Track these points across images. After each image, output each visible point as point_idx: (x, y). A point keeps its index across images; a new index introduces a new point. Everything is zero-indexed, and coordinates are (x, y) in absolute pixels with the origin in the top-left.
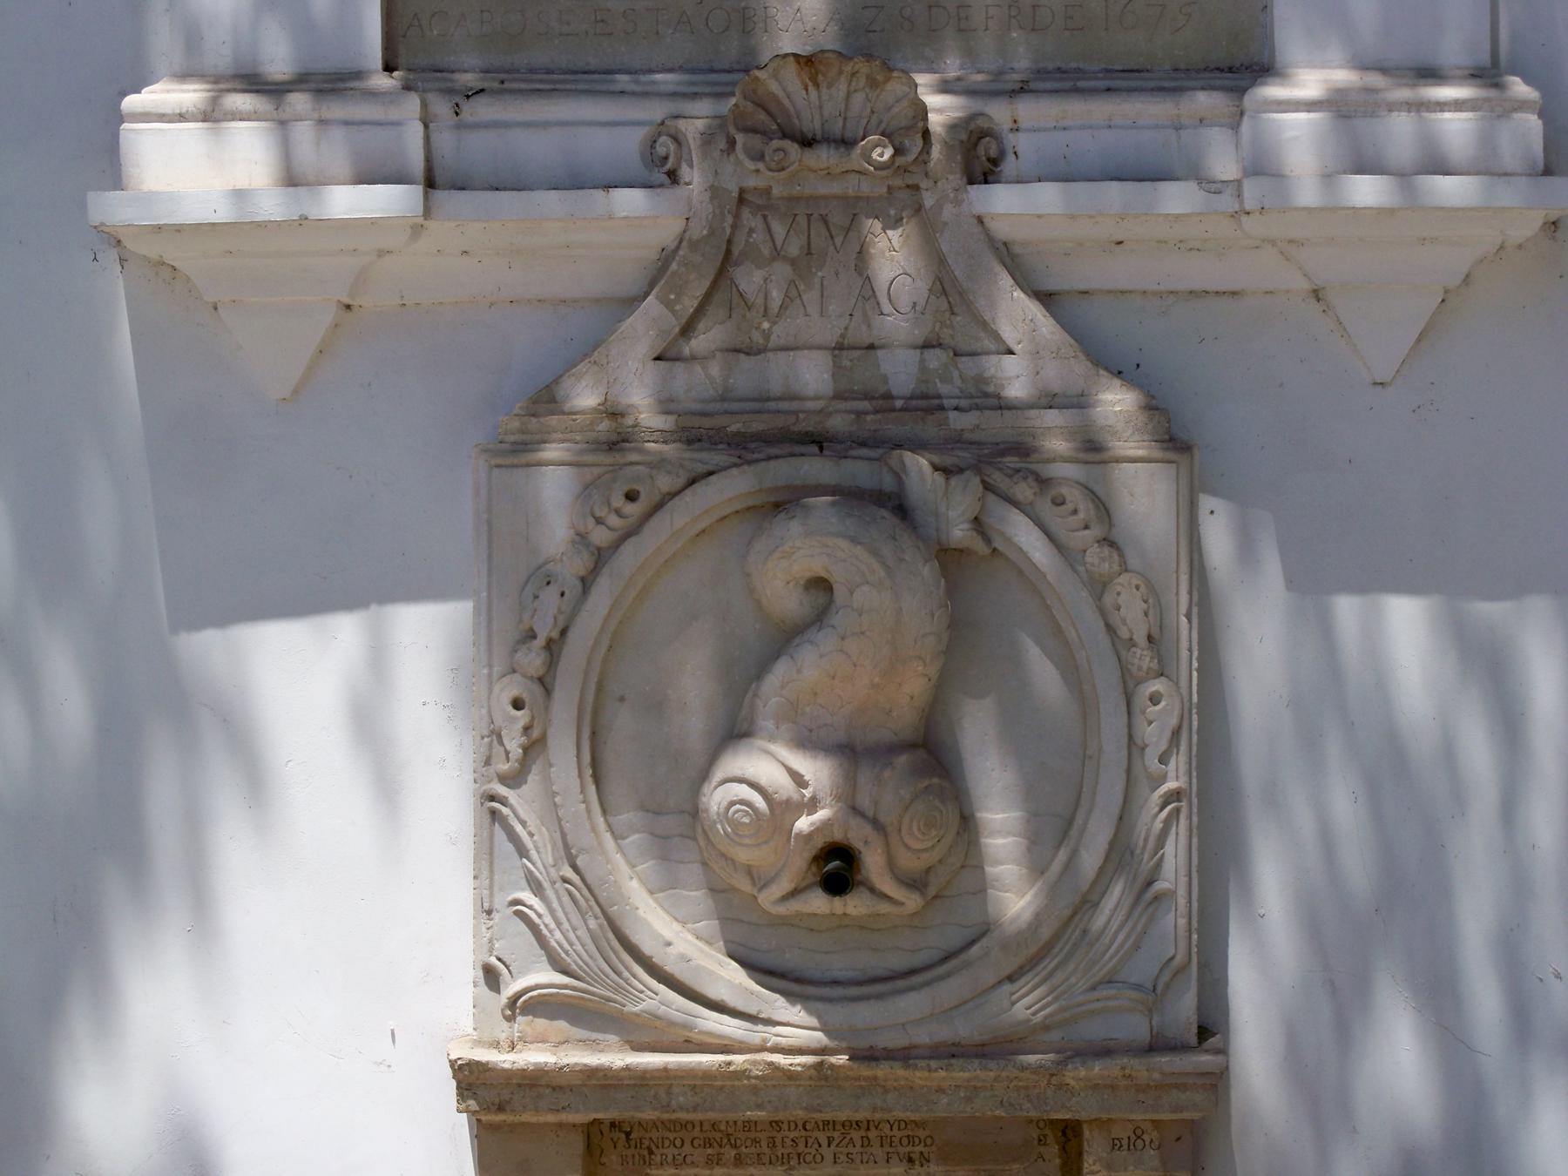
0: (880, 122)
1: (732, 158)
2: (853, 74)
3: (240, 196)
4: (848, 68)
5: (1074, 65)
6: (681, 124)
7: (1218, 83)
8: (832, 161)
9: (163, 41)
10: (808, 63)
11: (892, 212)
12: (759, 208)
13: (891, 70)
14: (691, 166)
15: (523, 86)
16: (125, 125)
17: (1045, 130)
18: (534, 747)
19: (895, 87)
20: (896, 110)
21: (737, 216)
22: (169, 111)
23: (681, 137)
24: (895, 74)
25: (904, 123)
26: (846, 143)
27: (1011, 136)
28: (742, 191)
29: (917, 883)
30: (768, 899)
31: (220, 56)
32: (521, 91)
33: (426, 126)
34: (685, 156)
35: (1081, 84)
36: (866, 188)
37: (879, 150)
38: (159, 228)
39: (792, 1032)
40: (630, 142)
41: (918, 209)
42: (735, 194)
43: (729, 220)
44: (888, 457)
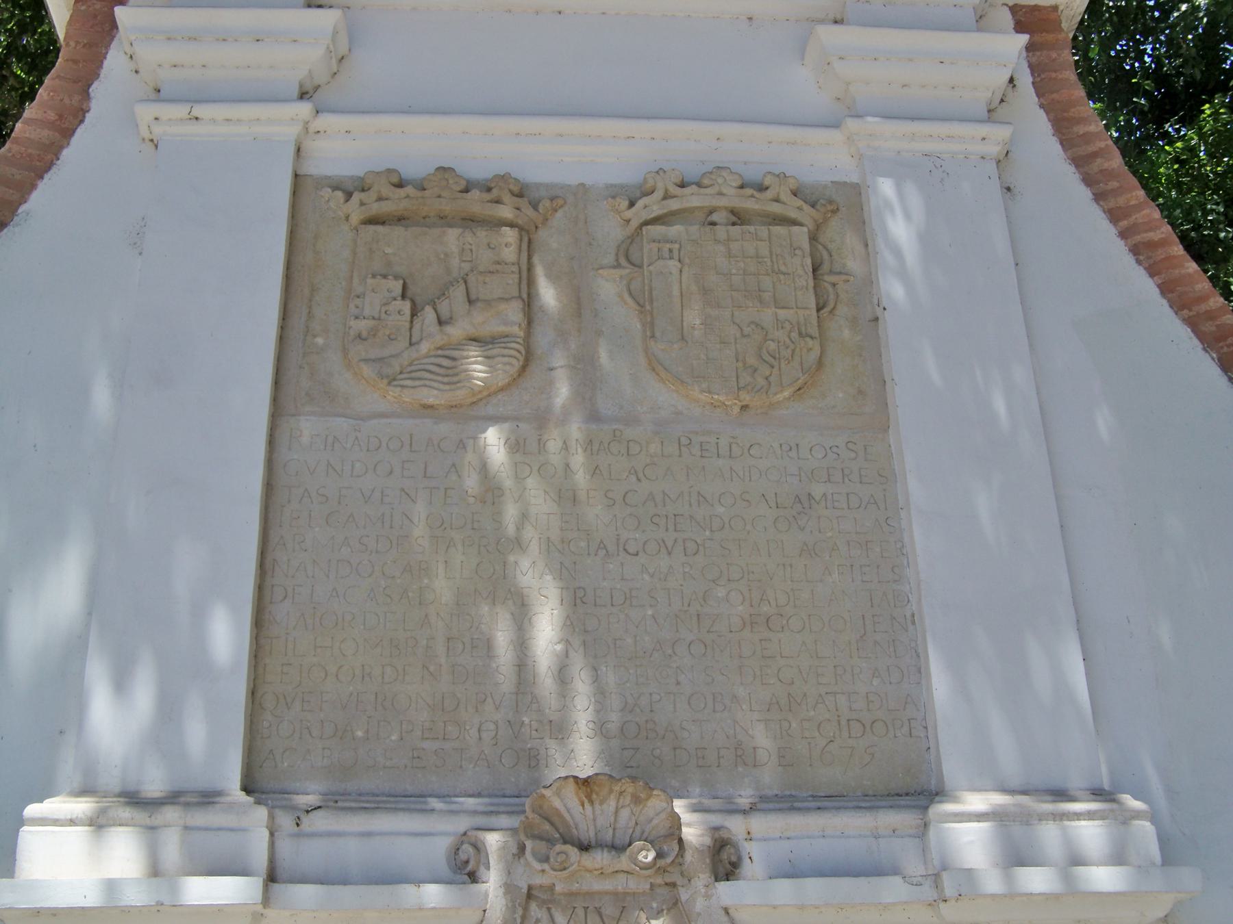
0: (643, 832)
1: (522, 860)
2: (621, 793)
3: (111, 886)
4: (617, 788)
5: (788, 793)
6: (481, 834)
7: (903, 803)
8: (605, 862)
9: (68, 770)
10: (585, 784)
11: (655, 905)
12: (544, 902)
13: (652, 789)
14: (488, 868)
15: (353, 805)
16: (25, 828)
17: (774, 839)
19: (656, 803)
20: (655, 822)
21: (526, 909)
22: (62, 817)
23: (480, 845)
24: (655, 792)
25: (663, 832)
26: (618, 848)
27: (746, 844)
28: (530, 888)
31: (111, 779)
32: (351, 809)
33: (272, 834)
34: (483, 860)
35: (796, 804)
36: (633, 885)
37: (644, 853)
38: (38, 912)
40: (440, 847)
41: (676, 902)
42: (525, 890)
43: (520, 911)
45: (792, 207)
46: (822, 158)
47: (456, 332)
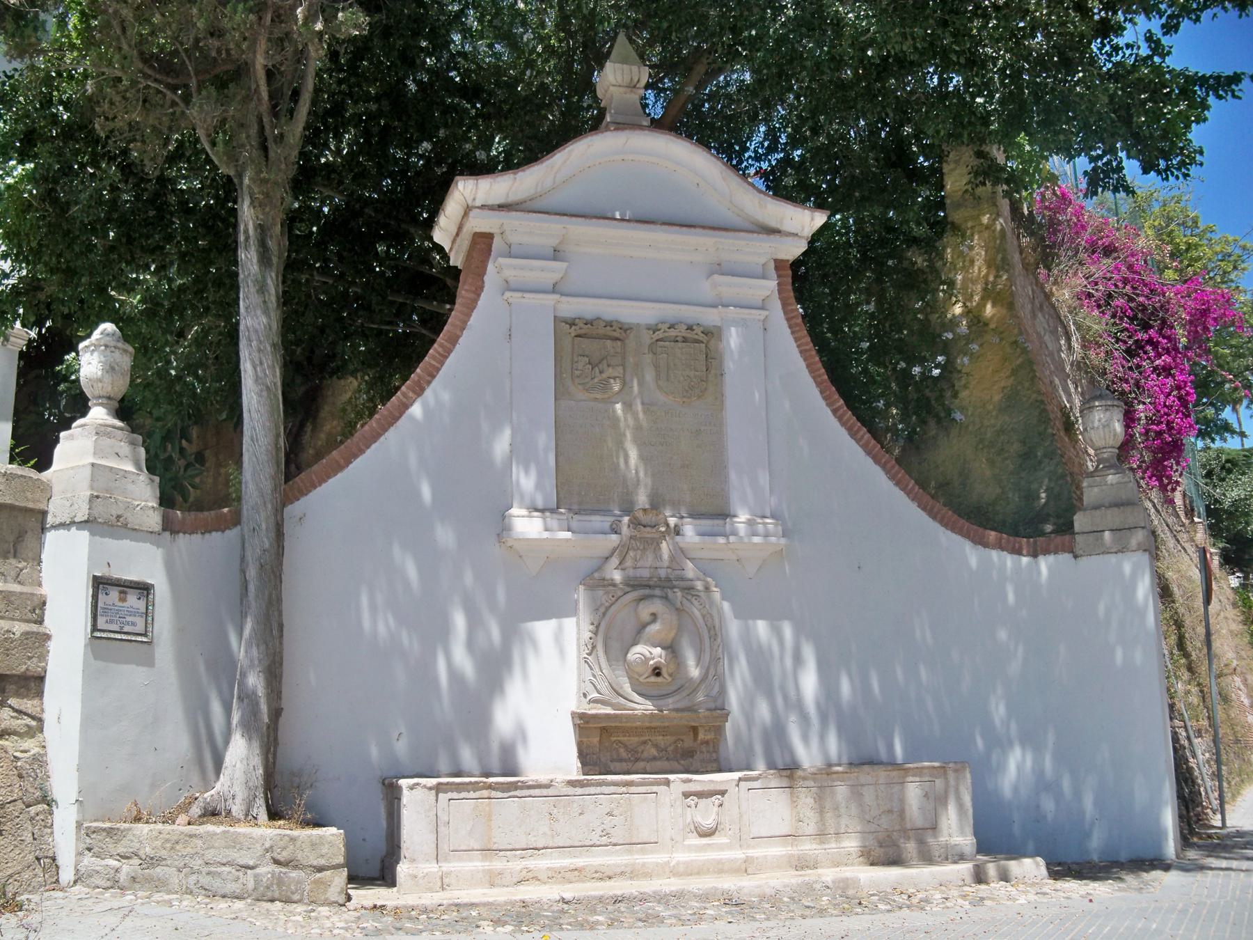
10: (645, 510)
18: (594, 647)
29: (670, 675)
30: (641, 679)
39: (643, 706)
40: (607, 526)
44: (661, 587)
45: (702, 337)
46: (710, 317)
47: (604, 376)
